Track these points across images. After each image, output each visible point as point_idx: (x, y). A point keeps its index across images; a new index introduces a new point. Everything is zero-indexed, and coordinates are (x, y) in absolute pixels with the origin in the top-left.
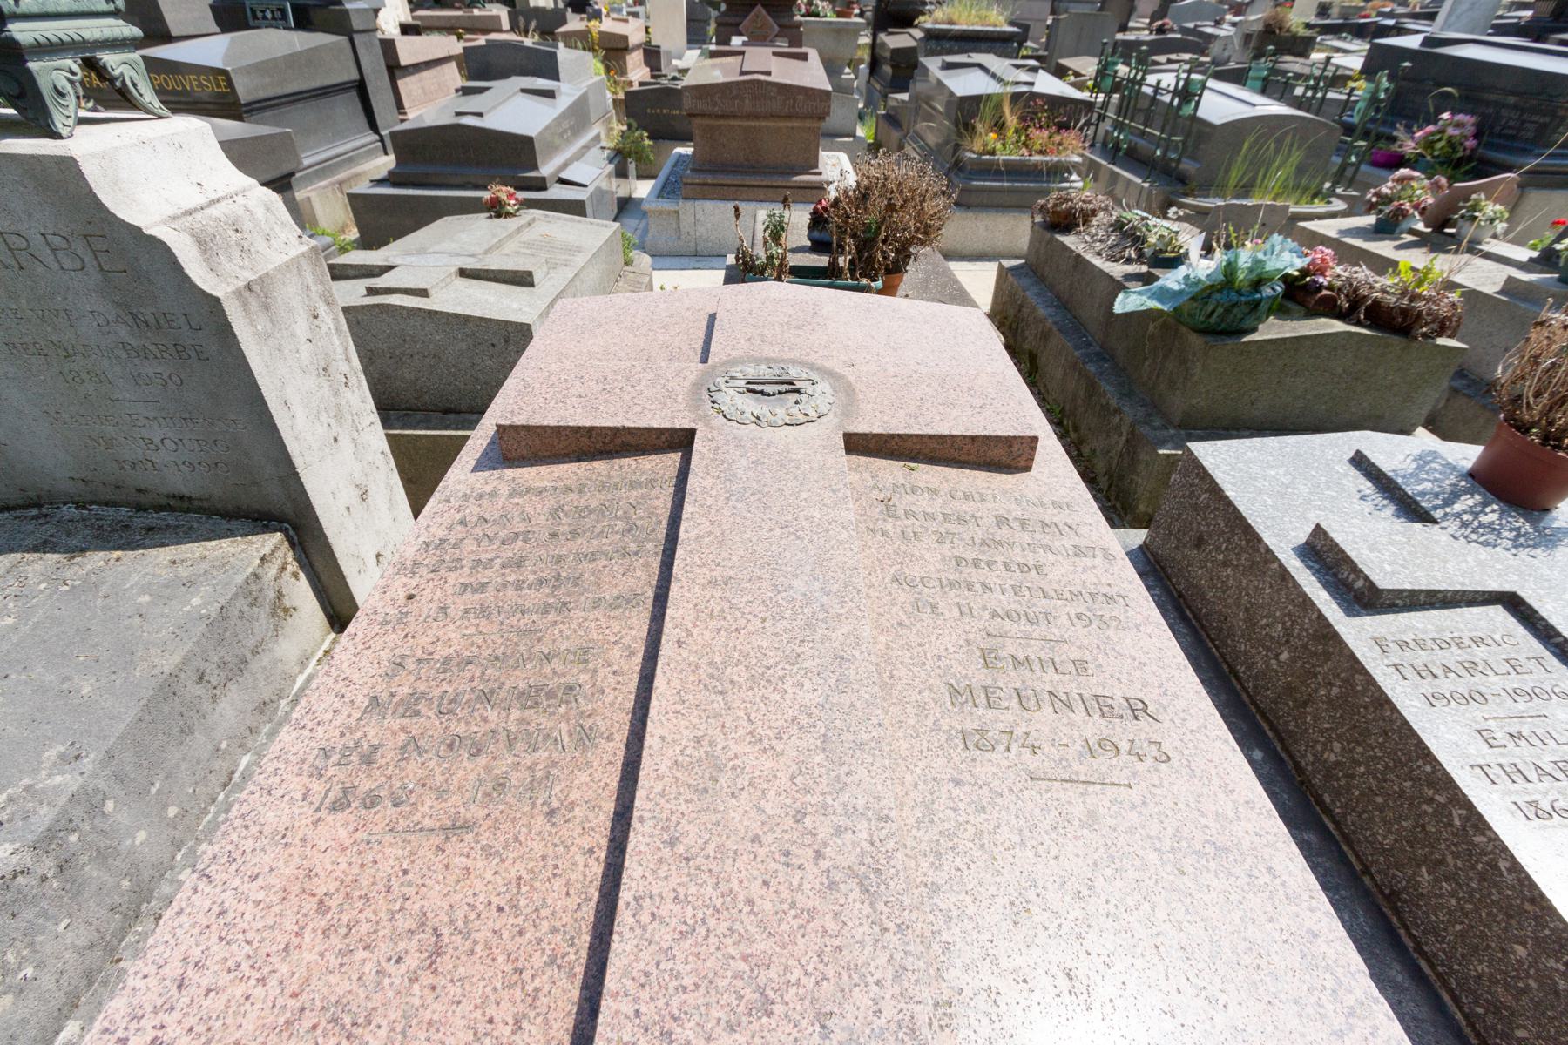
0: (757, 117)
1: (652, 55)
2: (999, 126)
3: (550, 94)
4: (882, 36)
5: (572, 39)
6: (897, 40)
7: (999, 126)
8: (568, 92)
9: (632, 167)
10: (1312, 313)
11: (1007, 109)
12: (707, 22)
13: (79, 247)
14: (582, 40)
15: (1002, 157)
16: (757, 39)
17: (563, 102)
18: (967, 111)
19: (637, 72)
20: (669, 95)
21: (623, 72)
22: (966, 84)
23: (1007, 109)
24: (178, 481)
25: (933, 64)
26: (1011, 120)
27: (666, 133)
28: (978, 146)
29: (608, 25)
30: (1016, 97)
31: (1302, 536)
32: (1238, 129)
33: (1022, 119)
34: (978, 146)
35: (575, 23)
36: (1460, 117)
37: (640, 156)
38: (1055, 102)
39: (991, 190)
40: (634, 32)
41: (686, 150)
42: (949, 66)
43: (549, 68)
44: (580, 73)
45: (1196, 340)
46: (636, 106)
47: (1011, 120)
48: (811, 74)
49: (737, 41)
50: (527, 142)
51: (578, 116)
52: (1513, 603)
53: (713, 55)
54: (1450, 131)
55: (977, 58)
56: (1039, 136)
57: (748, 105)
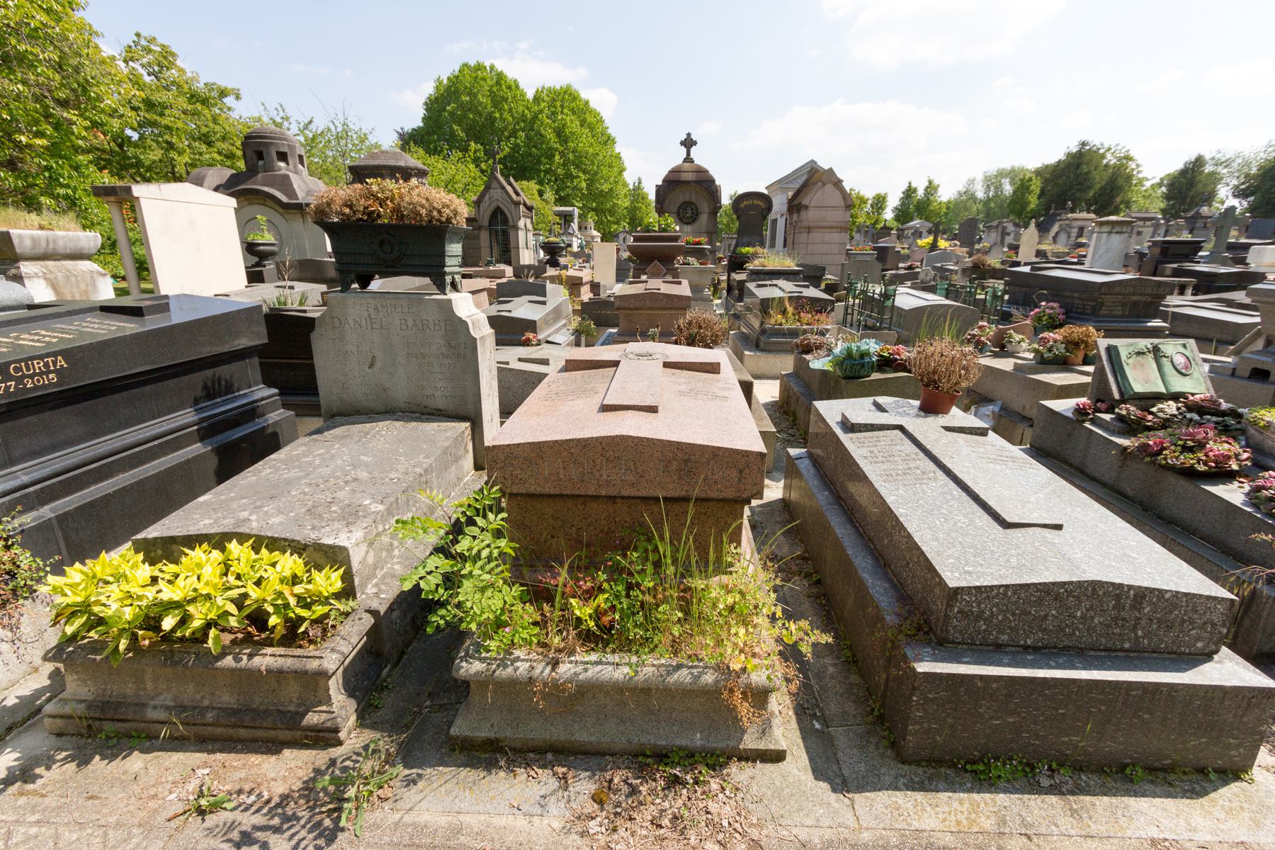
0: (652, 309)
1: (595, 287)
2: (784, 312)
3: (544, 303)
4: (734, 275)
5: (553, 279)
6: (739, 276)
7: (784, 312)
8: (551, 304)
9: (583, 339)
10: (896, 371)
11: (787, 304)
12: (629, 270)
13: (442, 324)
14: (556, 280)
15: (786, 327)
16: (654, 275)
17: (550, 306)
18: (765, 305)
19: (586, 295)
20: (605, 304)
21: (579, 296)
22: (763, 293)
23: (787, 304)
24: (440, 403)
25: (751, 286)
26: (790, 309)
27: (603, 323)
28: (773, 321)
29: (571, 272)
30: (790, 298)
31: (839, 419)
32: (919, 311)
33: (796, 308)
34: (773, 321)
35: (551, 272)
36: (1051, 304)
37: (588, 333)
38: (814, 301)
39: (781, 343)
40: (586, 275)
41: (614, 330)
42: (759, 286)
43: (541, 291)
44: (557, 295)
45: (843, 382)
46: (587, 310)
47: (790, 309)
48: (684, 289)
49: (644, 277)
50: (534, 322)
51: (557, 313)
52: (901, 428)
53: (631, 283)
54: (1048, 311)
55: (775, 282)
56: (806, 317)
57: (648, 304)
